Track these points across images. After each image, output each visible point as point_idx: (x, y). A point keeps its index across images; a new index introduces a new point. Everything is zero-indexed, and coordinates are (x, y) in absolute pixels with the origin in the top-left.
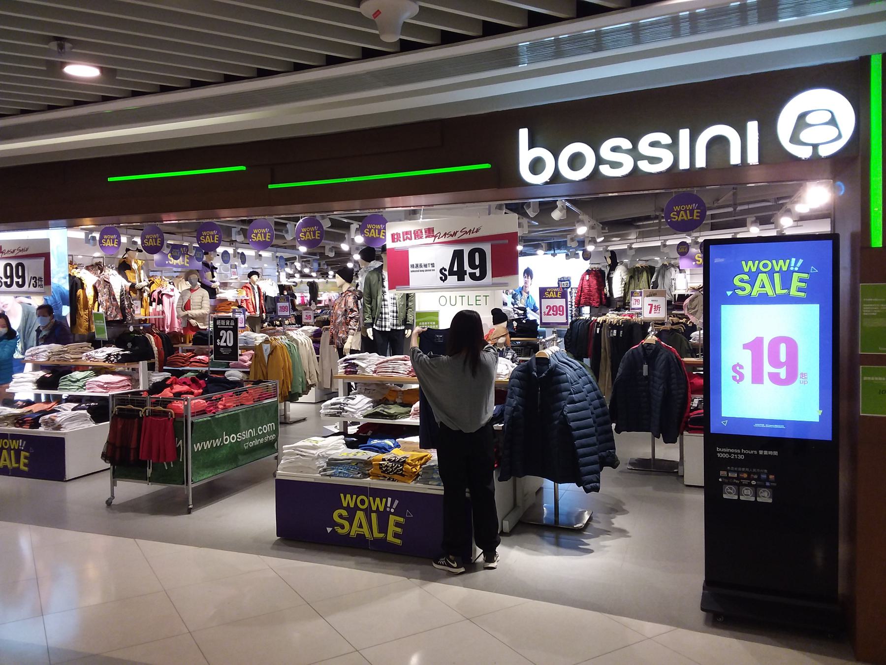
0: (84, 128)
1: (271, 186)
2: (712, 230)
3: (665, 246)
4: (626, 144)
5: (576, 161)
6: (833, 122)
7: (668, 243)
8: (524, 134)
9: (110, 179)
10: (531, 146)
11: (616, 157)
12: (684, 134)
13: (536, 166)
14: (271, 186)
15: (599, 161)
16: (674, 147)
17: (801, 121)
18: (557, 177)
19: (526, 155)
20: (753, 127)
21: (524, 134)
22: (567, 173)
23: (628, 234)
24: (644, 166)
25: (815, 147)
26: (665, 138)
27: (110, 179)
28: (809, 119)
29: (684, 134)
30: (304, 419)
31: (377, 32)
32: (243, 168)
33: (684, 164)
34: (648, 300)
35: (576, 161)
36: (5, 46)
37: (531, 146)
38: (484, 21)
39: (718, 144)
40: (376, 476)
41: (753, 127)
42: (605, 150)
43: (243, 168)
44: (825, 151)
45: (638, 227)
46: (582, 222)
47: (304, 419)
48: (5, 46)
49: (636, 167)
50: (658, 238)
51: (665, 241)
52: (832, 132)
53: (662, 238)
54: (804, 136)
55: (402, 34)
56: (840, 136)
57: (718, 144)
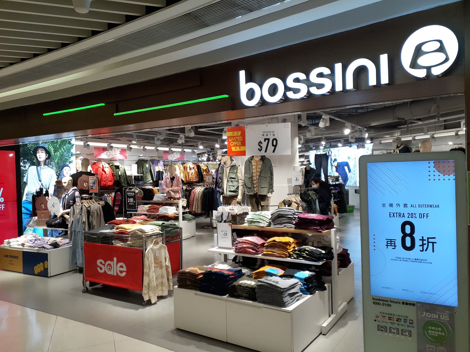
0: (8, 86)
1: (115, 114)
2: (445, 129)
3: (414, 139)
4: (302, 76)
5: (273, 90)
6: (442, 49)
7: (416, 138)
8: (242, 74)
9: (45, 115)
10: (247, 82)
11: (297, 86)
12: (338, 67)
13: (251, 95)
14: (115, 114)
15: (287, 89)
16: (332, 76)
17: (418, 52)
18: (263, 102)
19: (244, 87)
20: (384, 59)
21: (242, 74)
22: (268, 98)
23: (394, 133)
24: (314, 90)
25: (429, 69)
26: (326, 71)
27: (45, 115)
28: (424, 48)
29: (338, 67)
30: (433, 252)
31: (72, 7)
32: (103, 104)
33: (339, 88)
35: (273, 90)
36: (2, 47)
37: (247, 82)
38: (126, 15)
39: (361, 72)
40: (305, 258)
41: (384, 59)
42: (290, 81)
43: (103, 104)
44: (436, 72)
45: (400, 129)
46: (347, 127)
47: (433, 252)
48: (2, 47)
49: (309, 92)
50: (410, 135)
51: (415, 137)
52: (442, 57)
53: (412, 135)
54: (421, 61)
55: (91, 7)
56: (447, 60)
57: (361, 72)
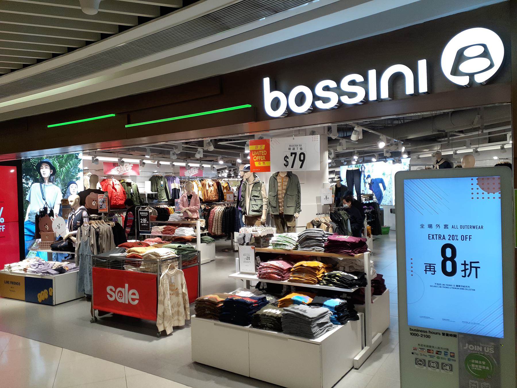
0: (9, 95)
1: (127, 126)
2: (489, 142)
3: (456, 154)
4: (332, 84)
5: (300, 99)
6: (486, 54)
7: (458, 152)
8: (266, 81)
9: (49, 126)
10: (271, 90)
11: (327, 95)
12: (372, 74)
13: (276, 104)
14: (127, 126)
15: (316, 98)
16: (365, 84)
17: (460, 57)
18: (289, 112)
19: (269, 96)
20: (422, 65)
21: (266, 81)
22: (295, 108)
23: (433, 147)
24: (345, 100)
25: (471, 76)
26: (359, 78)
27: (49, 126)
28: (466, 53)
29: (372, 74)
31: (80, 8)
32: (113, 115)
33: (373, 97)
34: (213, 190)
35: (300, 99)
36: (2, 52)
37: (271, 90)
39: (397, 79)
40: (335, 285)
41: (422, 65)
42: (319, 90)
43: (113, 115)
44: (480, 79)
45: (440, 142)
46: (382, 140)
48: (2, 52)
49: (339, 101)
50: (451, 149)
51: (456, 151)
52: (486, 62)
53: (453, 149)
54: (463, 67)
55: (100, 8)
56: (491, 66)
57: (397, 79)
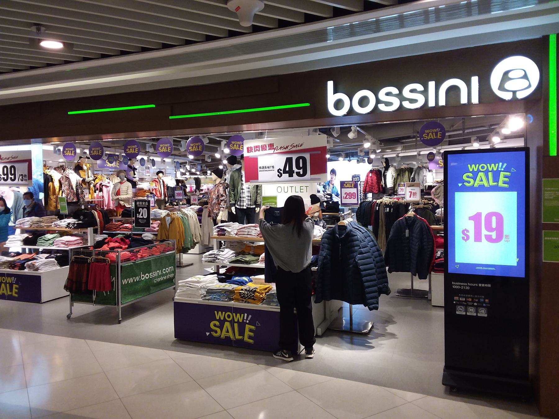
0: (53, 81)
1: (171, 117)
2: (449, 145)
3: (419, 155)
4: (395, 91)
5: (363, 102)
6: (525, 77)
7: (421, 153)
8: (330, 84)
9: (70, 113)
10: (335, 92)
11: (388, 99)
12: (432, 85)
13: (338, 104)
14: (171, 117)
15: (378, 101)
16: (425, 92)
17: (506, 76)
18: (351, 111)
19: (332, 98)
20: (475, 80)
21: (330, 84)
22: (358, 109)
23: (396, 148)
24: (406, 105)
25: (514, 92)
26: (420, 87)
27: (70, 113)
28: (510, 75)
29: (432, 85)
31: (238, 20)
32: (153, 106)
33: (432, 104)
35: (363, 102)
36: (3, 29)
37: (335, 92)
39: (453, 91)
40: (237, 300)
41: (475, 80)
42: (382, 94)
43: (153, 106)
44: (521, 95)
45: (403, 143)
46: (367, 140)
48: (3, 29)
49: (401, 105)
50: (415, 150)
51: (420, 152)
52: (525, 83)
53: (417, 150)
54: (507, 86)
55: (253, 22)
56: (530, 86)
57: (453, 91)
